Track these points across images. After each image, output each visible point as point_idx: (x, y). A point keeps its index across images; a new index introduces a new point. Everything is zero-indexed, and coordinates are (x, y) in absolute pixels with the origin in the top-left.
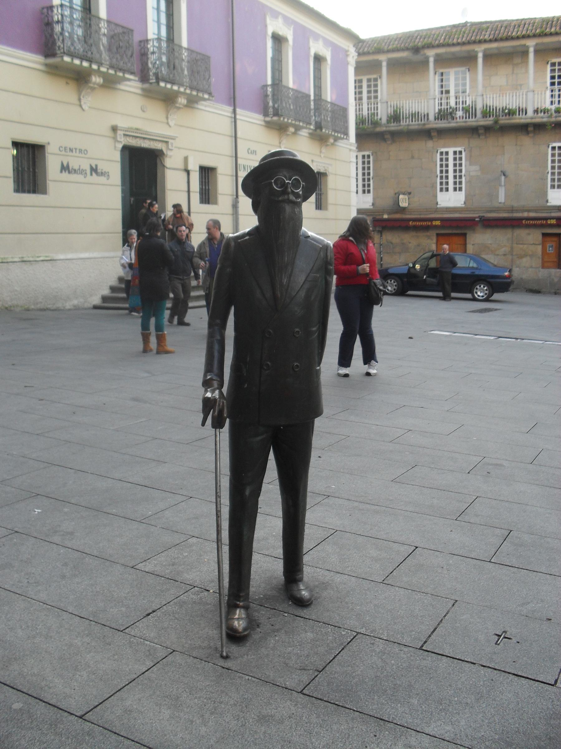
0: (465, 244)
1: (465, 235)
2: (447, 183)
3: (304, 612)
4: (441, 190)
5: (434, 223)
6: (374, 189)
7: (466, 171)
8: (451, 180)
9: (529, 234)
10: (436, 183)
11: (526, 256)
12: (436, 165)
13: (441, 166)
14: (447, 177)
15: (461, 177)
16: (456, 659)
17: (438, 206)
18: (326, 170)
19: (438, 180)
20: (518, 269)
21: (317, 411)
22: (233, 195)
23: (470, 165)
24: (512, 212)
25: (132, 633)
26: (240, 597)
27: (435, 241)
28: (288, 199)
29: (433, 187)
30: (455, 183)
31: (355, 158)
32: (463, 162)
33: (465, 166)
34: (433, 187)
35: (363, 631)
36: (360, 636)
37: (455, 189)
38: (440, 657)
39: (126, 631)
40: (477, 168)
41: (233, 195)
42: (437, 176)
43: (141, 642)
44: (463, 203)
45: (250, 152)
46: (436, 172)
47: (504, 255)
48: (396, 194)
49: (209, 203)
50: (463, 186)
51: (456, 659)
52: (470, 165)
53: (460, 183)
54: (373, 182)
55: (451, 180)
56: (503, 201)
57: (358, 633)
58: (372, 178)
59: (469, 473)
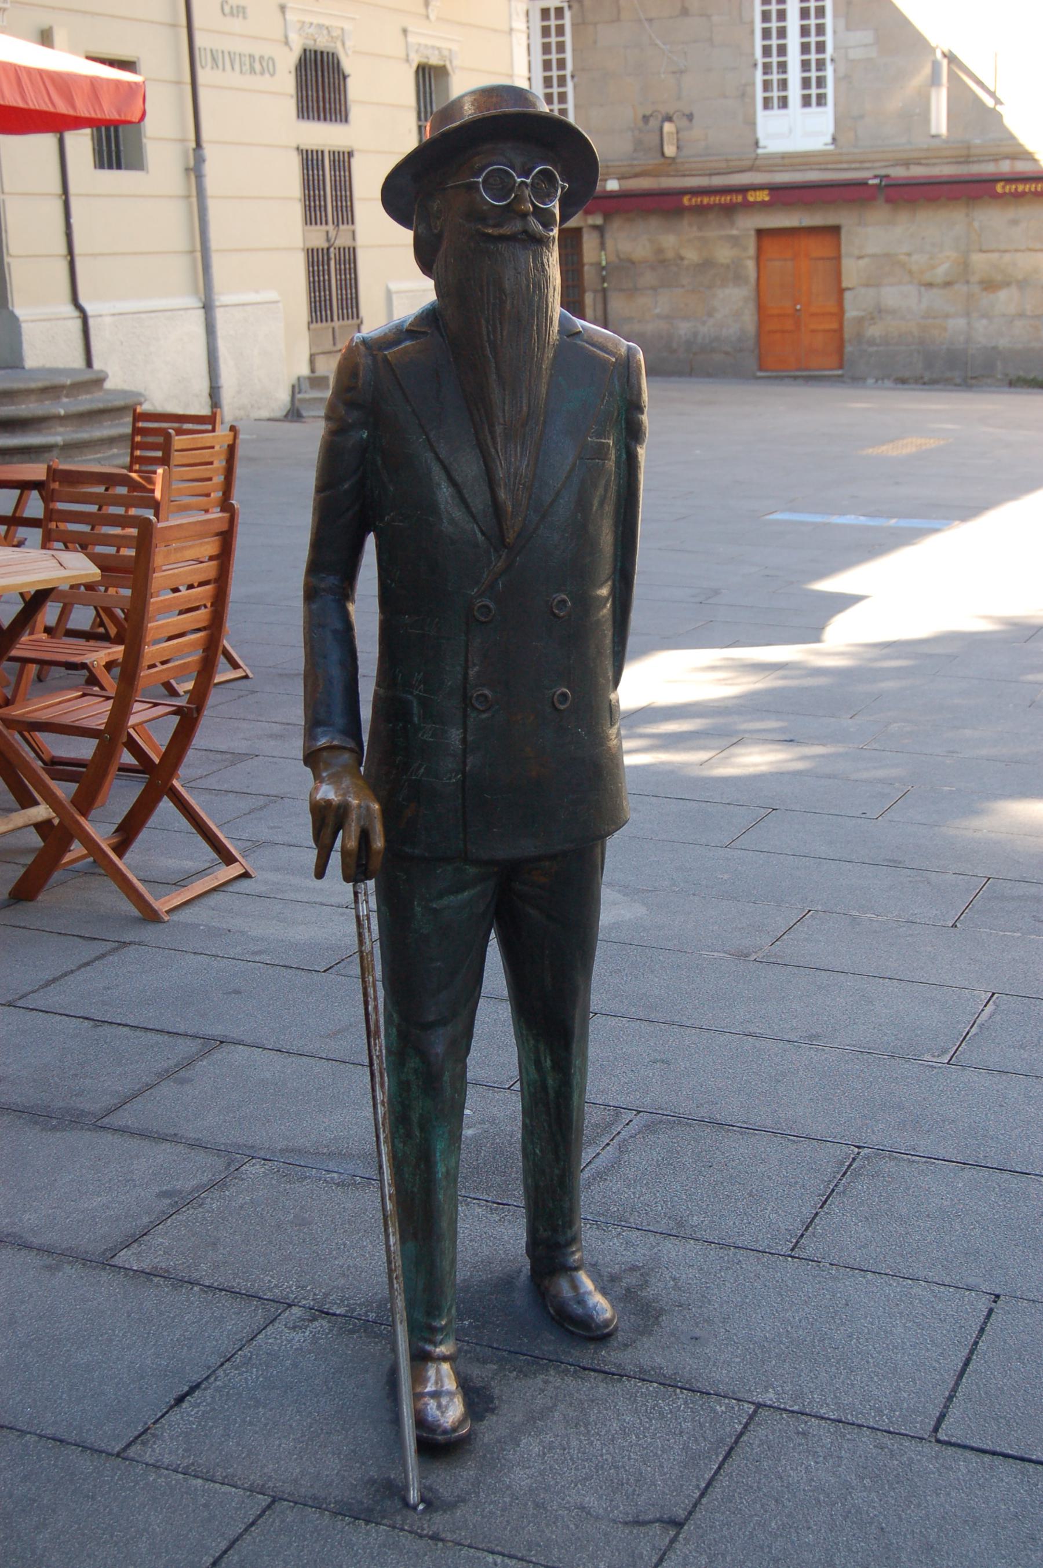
0: (838, 258)
1: (835, 230)
2: (783, 84)
3: (586, 1355)
4: (767, 104)
5: (751, 197)
6: (576, 107)
7: (836, 48)
8: (794, 75)
9: (1015, 222)
10: (754, 84)
11: (1008, 284)
12: (752, 32)
13: (766, 34)
14: (783, 67)
15: (821, 65)
16: (1030, 1461)
17: (760, 151)
18: (442, 57)
19: (759, 77)
20: (984, 322)
21: (614, 820)
22: (183, 141)
23: (848, 28)
24: (967, 162)
25: (148, 1458)
26: (434, 1330)
27: (752, 251)
28: (525, 232)
29: (743, 95)
30: (806, 83)
31: (523, 19)
32: (829, 21)
33: (835, 32)
34: (743, 95)
35: (769, 1397)
36: (763, 1413)
37: (806, 101)
38: (987, 1458)
39: (131, 1452)
40: (866, 36)
41: (183, 141)
42: (755, 65)
43: (178, 1481)
44: (829, 140)
45: (227, 9)
46: (753, 54)
47: (948, 284)
48: (646, 119)
49: (119, 167)
50: (830, 90)
51: (1030, 1461)
52: (848, 28)
53: (821, 82)
54: (575, 87)
55: (794, 75)
56: (943, 130)
57: (759, 1406)
58: (573, 77)
59: (954, 926)
